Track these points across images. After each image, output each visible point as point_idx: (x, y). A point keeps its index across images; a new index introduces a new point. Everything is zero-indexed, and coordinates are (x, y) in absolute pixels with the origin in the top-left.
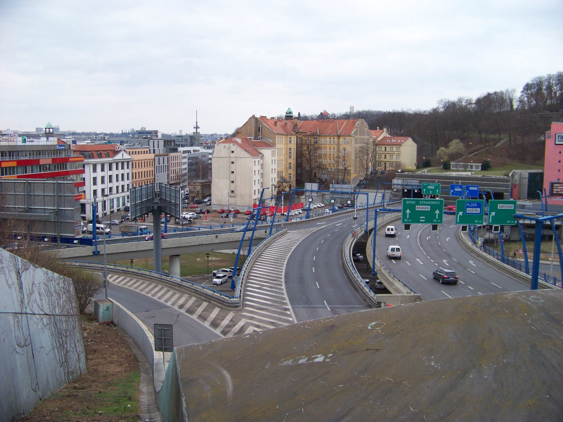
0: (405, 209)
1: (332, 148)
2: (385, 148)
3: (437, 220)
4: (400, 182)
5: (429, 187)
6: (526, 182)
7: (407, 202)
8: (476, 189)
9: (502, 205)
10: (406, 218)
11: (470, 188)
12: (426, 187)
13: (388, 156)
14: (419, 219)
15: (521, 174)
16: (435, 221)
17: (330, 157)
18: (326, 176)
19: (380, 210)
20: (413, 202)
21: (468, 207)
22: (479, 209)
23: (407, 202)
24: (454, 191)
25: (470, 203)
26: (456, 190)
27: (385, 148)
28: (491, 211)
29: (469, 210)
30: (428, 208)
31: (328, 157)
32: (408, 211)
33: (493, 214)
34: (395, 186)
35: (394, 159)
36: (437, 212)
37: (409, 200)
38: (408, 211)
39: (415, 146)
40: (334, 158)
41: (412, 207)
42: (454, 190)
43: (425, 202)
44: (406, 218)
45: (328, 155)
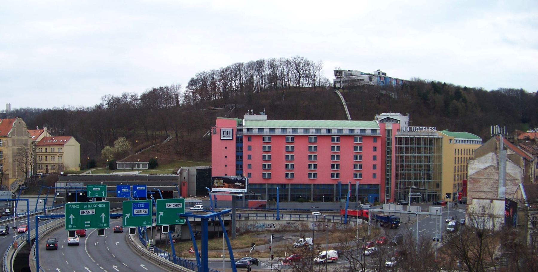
0: (68, 215)
2: (46, 149)
3: (104, 224)
4: (63, 185)
5: (94, 189)
7: (70, 207)
8: (144, 188)
9: (170, 204)
11: (138, 188)
12: (91, 189)
15: (190, 171)
16: (101, 225)
20: (77, 207)
22: (147, 210)
23: (70, 207)
25: (137, 204)
26: (123, 190)
27: (46, 149)
28: (159, 210)
29: (137, 212)
30: (93, 212)
32: (72, 216)
33: (162, 213)
34: (59, 190)
35: (56, 160)
36: (103, 215)
37: (71, 204)
38: (72, 216)
39: (78, 146)
41: (76, 212)
42: (121, 190)
43: (89, 206)
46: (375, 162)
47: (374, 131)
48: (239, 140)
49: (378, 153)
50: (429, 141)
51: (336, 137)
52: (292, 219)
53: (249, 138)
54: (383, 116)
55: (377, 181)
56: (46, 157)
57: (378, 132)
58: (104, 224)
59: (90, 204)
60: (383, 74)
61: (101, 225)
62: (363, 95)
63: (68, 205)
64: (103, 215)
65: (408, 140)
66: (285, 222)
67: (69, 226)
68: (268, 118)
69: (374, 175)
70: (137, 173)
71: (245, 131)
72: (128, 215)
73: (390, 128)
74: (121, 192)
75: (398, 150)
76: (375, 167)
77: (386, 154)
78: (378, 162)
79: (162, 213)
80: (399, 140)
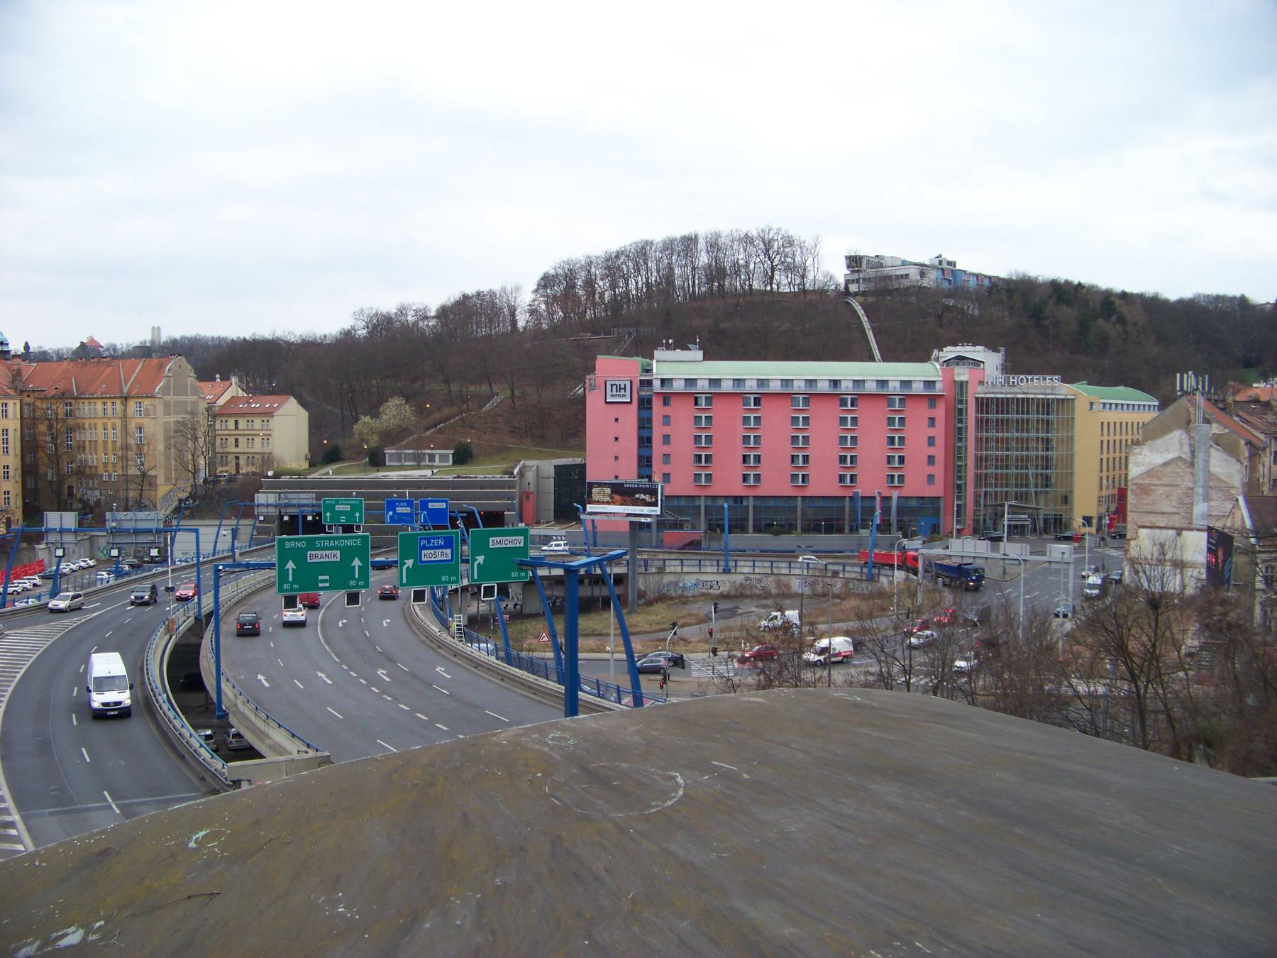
0: (283, 561)
1: (109, 427)
2: (236, 422)
3: (358, 580)
4: (272, 498)
5: (338, 508)
6: (551, 483)
7: (288, 545)
8: (443, 506)
9: (498, 539)
10: (354, 578)
11: (431, 506)
13: (242, 441)
14: (317, 581)
15: (540, 468)
16: (352, 583)
17: (105, 449)
18: (97, 493)
19: (225, 566)
21: (425, 548)
22: (449, 551)
23: (288, 545)
24: (395, 513)
25: (429, 540)
26: (399, 510)
27: (236, 422)
28: (476, 552)
29: (428, 555)
30: (336, 556)
31: (100, 448)
32: (290, 565)
36: (357, 563)
38: (290, 565)
39: (303, 415)
40: (114, 449)
41: (299, 556)
42: (394, 511)
44: (287, 582)
45: (100, 442)
46: (932, 451)
47: (929, 384)
48: (645, 404)
49: (939, 431)
50: (1046, 406)
51: (897, 398)
52: (757, 571)
53: (666, 399)
54: (950, 352)
55: (937, 490)
56: (237, 440)
57: (939, 386)
58: (358, 580)
59: (330, 539)
60: (949, 263)
61: (352, 583)
62: (906, 310)
63: (282, 542)
64: (357, 563)
65: (1003, 405)
66: (742, 577)
67: (285, 586)
68: (705, 358)
69: (931, 478)
70: (428, 473)
71: (657, 384)
72: (409, 563)
73: (964, 378)
74: (395, 513)
75: (980, 423)
76: (931, 460)
77: (956, 434)
78: (939, 451)
79: (481, 559)
80: (983, 404)
